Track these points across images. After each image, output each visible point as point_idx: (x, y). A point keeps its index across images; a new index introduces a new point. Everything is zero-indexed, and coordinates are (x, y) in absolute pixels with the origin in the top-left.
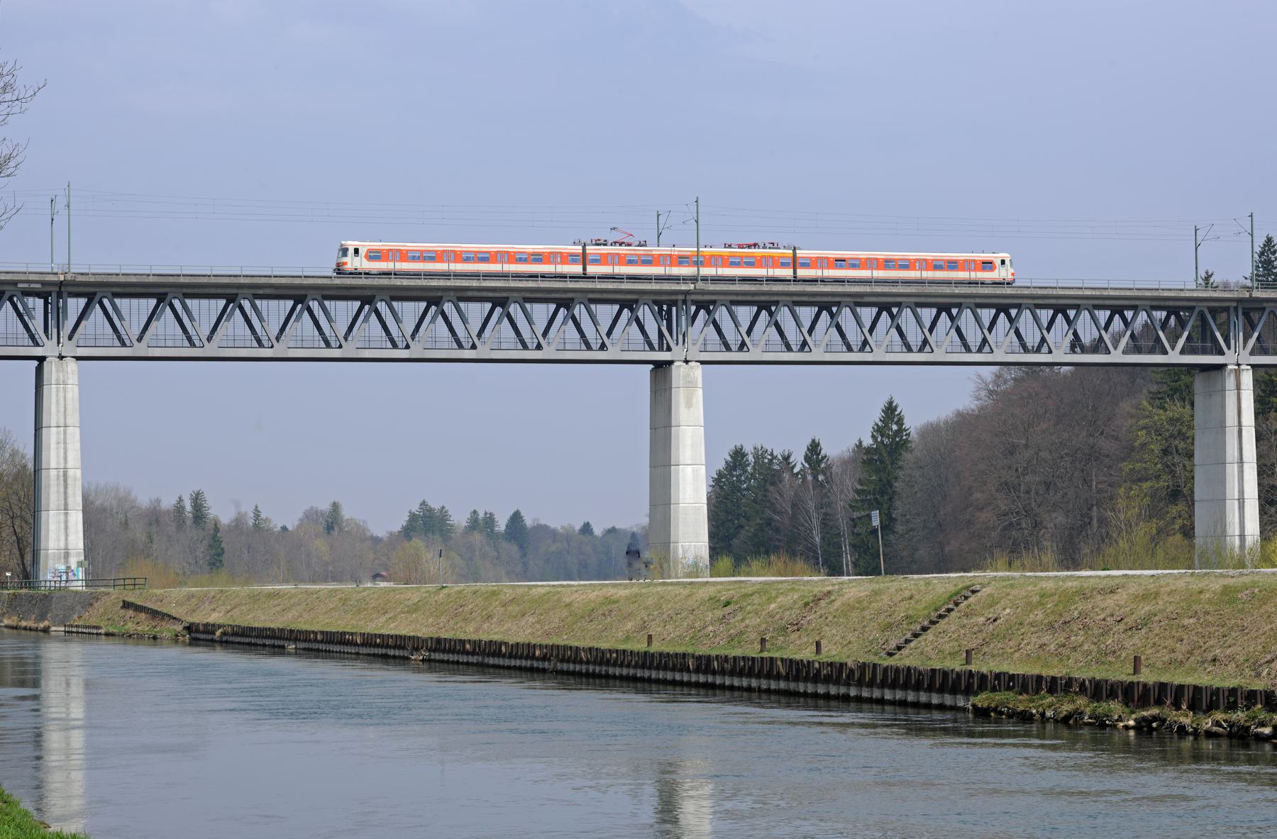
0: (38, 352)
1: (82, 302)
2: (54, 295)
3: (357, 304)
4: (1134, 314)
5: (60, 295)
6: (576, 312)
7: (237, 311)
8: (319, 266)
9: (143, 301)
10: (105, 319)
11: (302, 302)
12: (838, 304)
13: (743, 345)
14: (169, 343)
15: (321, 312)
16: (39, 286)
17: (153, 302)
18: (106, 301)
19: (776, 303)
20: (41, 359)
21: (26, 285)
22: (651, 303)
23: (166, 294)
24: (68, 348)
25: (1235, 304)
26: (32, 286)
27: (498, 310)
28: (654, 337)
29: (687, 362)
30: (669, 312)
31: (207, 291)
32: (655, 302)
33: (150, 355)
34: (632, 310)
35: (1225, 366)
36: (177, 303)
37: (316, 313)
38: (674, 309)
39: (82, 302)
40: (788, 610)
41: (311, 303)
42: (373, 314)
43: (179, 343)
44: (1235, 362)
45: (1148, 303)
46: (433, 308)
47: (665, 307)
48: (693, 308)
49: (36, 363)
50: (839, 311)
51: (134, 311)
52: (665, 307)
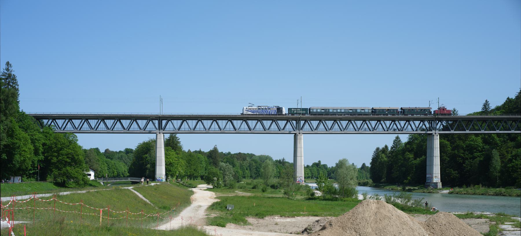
0: (295, 132)
1: (304, 122)
2: (298, 120)
3: (362, 121)
5: (299, 120)
6: (396, 122)
7: (336, 124)
8: (237, 112)
9: (316, 121)
10: (313, 125)
11: (350, 121)
12: (442, 120)
13: (387, 131)
14: (307, 130)
15: (369, 123)
16: (155, 118)
17: (286, 121)
18: (309, 121)
19: (424, 120)
20: (295, 134)
21: (152, 118)
22: (427, 120)
23: (321, 120)
24: (301, 131)
25: (435, 119)
26: (153, 118)
27: (407, 123)
28: (157, 126)
29: (299, 133)
30: (432, 123)
31: (417, 119)
32: (429, 120)
33: (94, 132)
34: (423, 122)
35: (432, 134)
36: (323, 122)
37: (353, 123)
38: (433, 122)
39: (304, 122)
40: (123, 176)
41: (338, 121)
42: (366, 124)
43: (324, 130)
44: (435, 133)
45: (413, 119)
46: (364, 122)
47: (431, 121)
48: (437, 122)
49: (294, 134)
50: (425, 122)
51: (315, 124)
52: (431, 121)
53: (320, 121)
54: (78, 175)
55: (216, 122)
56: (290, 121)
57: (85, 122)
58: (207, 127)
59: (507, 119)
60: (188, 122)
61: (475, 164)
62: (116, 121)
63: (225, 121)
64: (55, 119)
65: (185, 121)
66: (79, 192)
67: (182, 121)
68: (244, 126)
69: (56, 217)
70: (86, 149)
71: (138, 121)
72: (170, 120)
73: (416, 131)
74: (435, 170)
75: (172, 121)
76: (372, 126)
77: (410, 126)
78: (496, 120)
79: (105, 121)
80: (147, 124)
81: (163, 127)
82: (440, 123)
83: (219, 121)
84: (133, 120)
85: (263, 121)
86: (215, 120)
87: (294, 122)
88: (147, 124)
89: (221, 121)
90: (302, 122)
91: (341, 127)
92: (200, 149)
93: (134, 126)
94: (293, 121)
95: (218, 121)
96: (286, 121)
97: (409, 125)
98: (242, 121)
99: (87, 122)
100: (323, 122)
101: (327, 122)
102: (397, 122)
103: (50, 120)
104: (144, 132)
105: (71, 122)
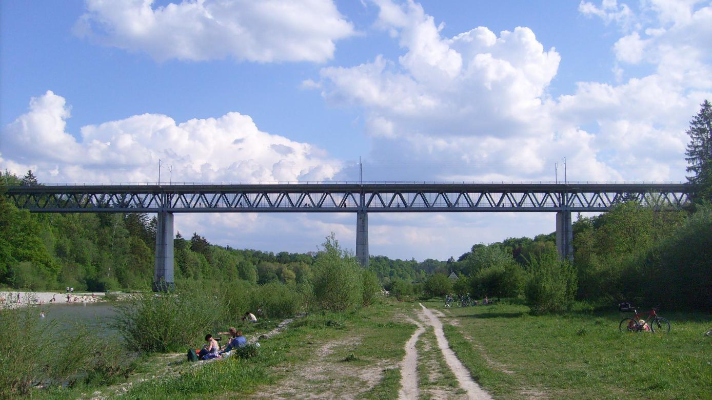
4: (503, 194)
21: (73, 191)
23: (506, 191)
54: (306, 350)
55: (443, 195)
56: (465, 194)
57: (243, 197)
58: (475, 201)
59: (351, 190)
60: (206, 196)
61: (101, 339)
62: (304, 194)
63: (190, 194)
64: (223, 193)
67: (371, 194)
72: (350, 192)
73: (84, 207)
75: (353, 194)
76: (156, 201)
77: (538, 200)
78: (174, 193)
79: (268, 194)
80: (523, 199)
81: (366, 203)
82: (641, 196)
84: (304, 194)
85: (424, 194)
86: (441, 193)
88: (523, 199)
89: (429, 194)
90: (129, 196)
92: (413, 258)
93: (328, 202)
95: (380, 194)
97: (599, 198)
99: (223, 198)
100: (465, 194)
101: (492, 194)
102: (602, 194)
103: (610, 205)
104: (239, 203)
105: (488, 196)
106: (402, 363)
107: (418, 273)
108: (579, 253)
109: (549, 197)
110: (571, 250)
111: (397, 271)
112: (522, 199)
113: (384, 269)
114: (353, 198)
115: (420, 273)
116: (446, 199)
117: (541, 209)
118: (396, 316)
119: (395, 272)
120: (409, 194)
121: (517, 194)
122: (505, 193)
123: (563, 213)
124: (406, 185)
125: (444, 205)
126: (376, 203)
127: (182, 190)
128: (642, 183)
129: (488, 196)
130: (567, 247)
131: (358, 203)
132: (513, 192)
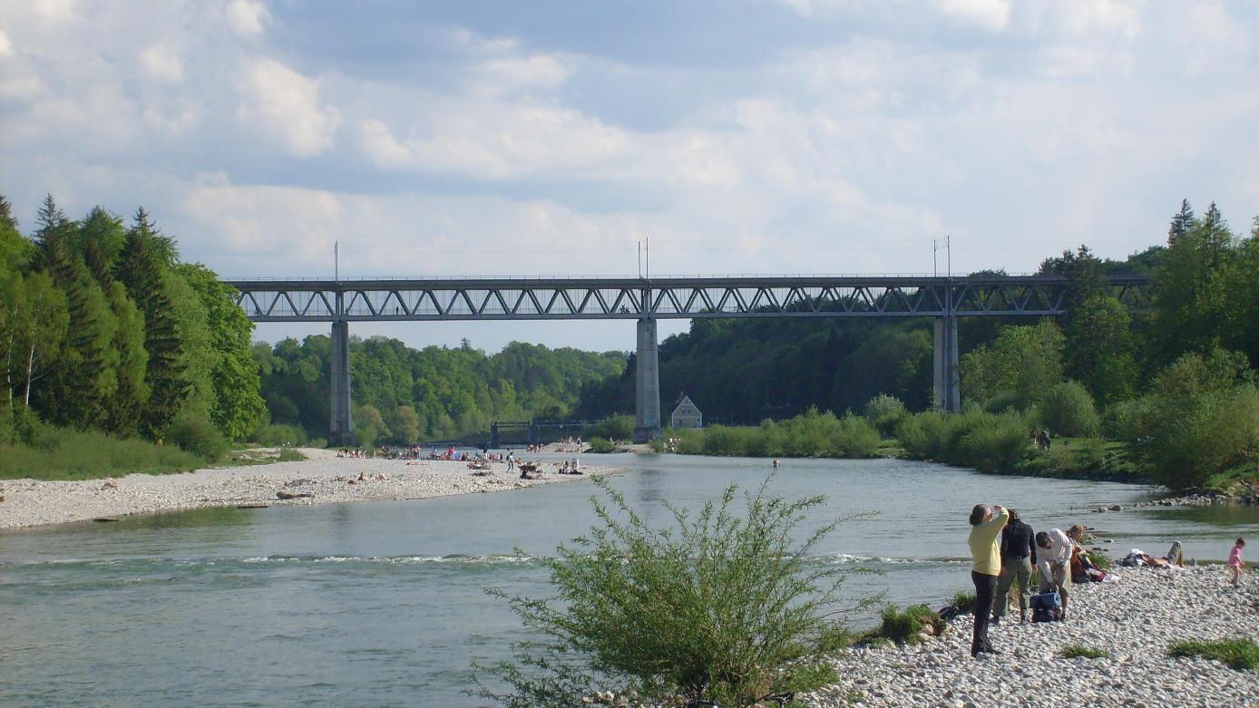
1: (659, 291)
17: (586, 291)
39: (659, 291)
48: (240, 294)
53: (697, 290)
65: (490, 290)
66: (1232, 530)
68: (394, 302)
69: (356, 599)
70: (435, 347)
71: (291, 294)
74: (817, 466)
75: (288, 293)
83: (405, 292)
85: (568, 291)
87: (637, 293)
88: (692, 298)
89: (262, 293)
90: (656, 293)
91: (743, 306)
94: (634, 291)
96: (586, 291)
98: (355, 293)
100: (767, 290)
105: (704, 294)
106: (1048, 533)
107: (494, 391)
108: (965, 381)
109: (731, 294)
110: (956, 377)
111: (435, 384)
112: (690, 299)
113: (396, 380)
114: (253, 300)
115: (500, 392)
116: (600, 299)
117: (609, 314)
118: (184, 416)
119: (432, 389)
120: (266, 293)
121: (780, 289)
122: (697, 290)
123: (647, 321)
124: (673, 279)
125: (533, 310)
126: (666, 305)
127: (361, 287)
128: (883, 276)
129: (704, 294)
130: (950, 375)
131: (334, 308)
132: (774, 287)
